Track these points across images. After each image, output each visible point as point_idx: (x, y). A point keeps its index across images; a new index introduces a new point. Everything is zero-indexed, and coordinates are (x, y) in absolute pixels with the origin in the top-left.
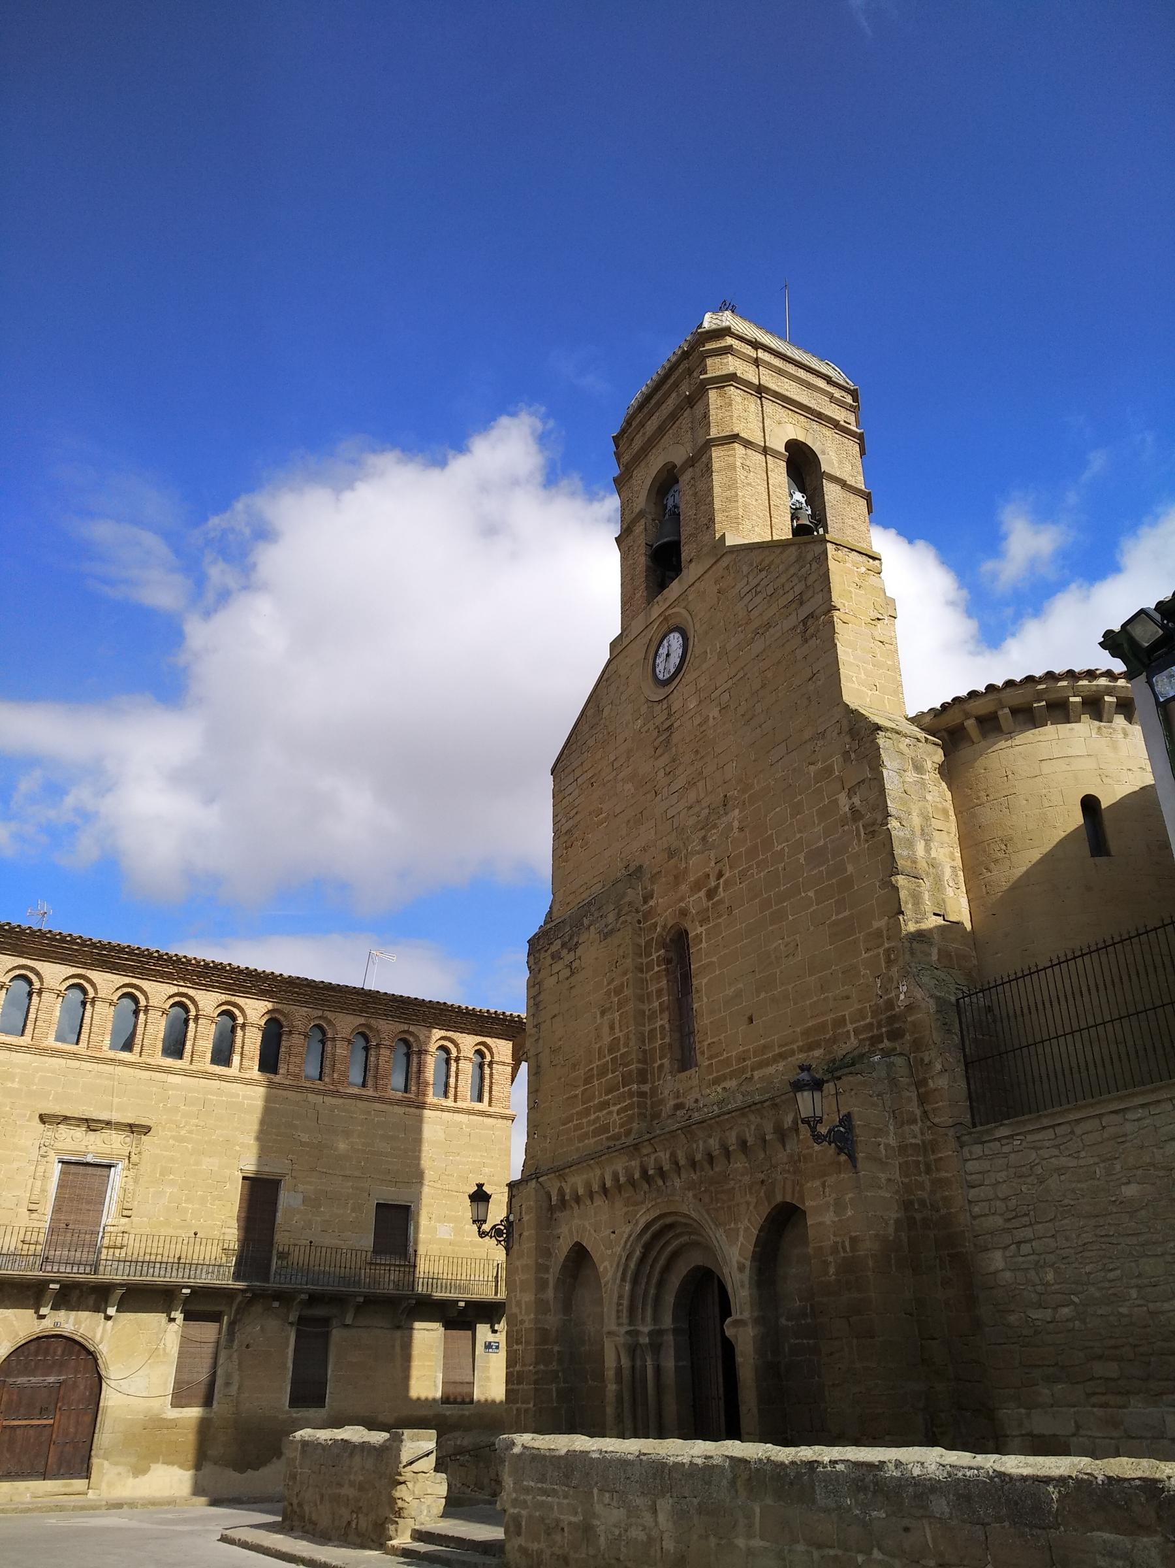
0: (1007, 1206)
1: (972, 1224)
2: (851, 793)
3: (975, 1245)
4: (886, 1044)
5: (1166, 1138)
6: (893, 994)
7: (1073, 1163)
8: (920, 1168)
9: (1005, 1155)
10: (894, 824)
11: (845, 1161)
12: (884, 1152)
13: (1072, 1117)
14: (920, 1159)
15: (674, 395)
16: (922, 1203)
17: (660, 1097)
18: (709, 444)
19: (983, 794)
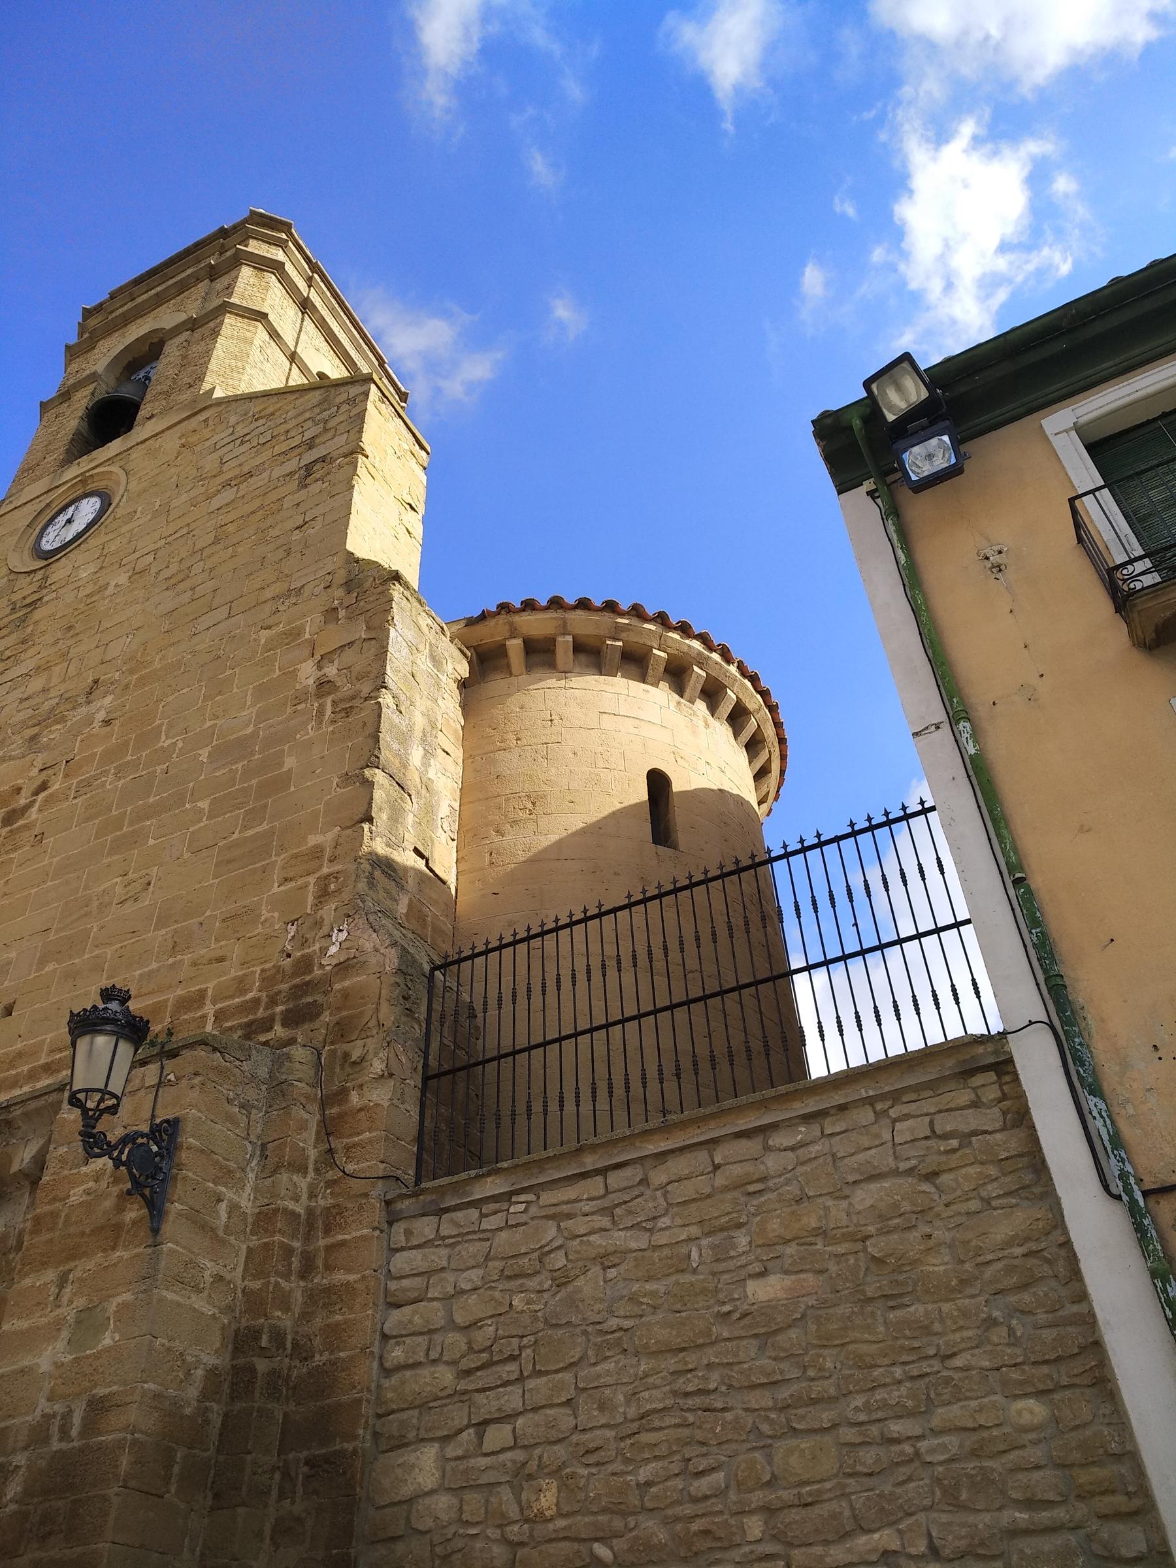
0: (469, 1343)
1: (379, 1387)
3: (376, 1435)
4: (279, 1031)
5: (858, 1177)
6: (317, 947)
7: (637, 1241)
8: (290, 1264)
9: (489, 1235)
10: (388, 701)
11: (134, 1223)
12: (224, 1215)
13: (651, 1148)
14: (296, 1244)
16: (278, 1337)
18: (226, 308)
19: (511, 737)
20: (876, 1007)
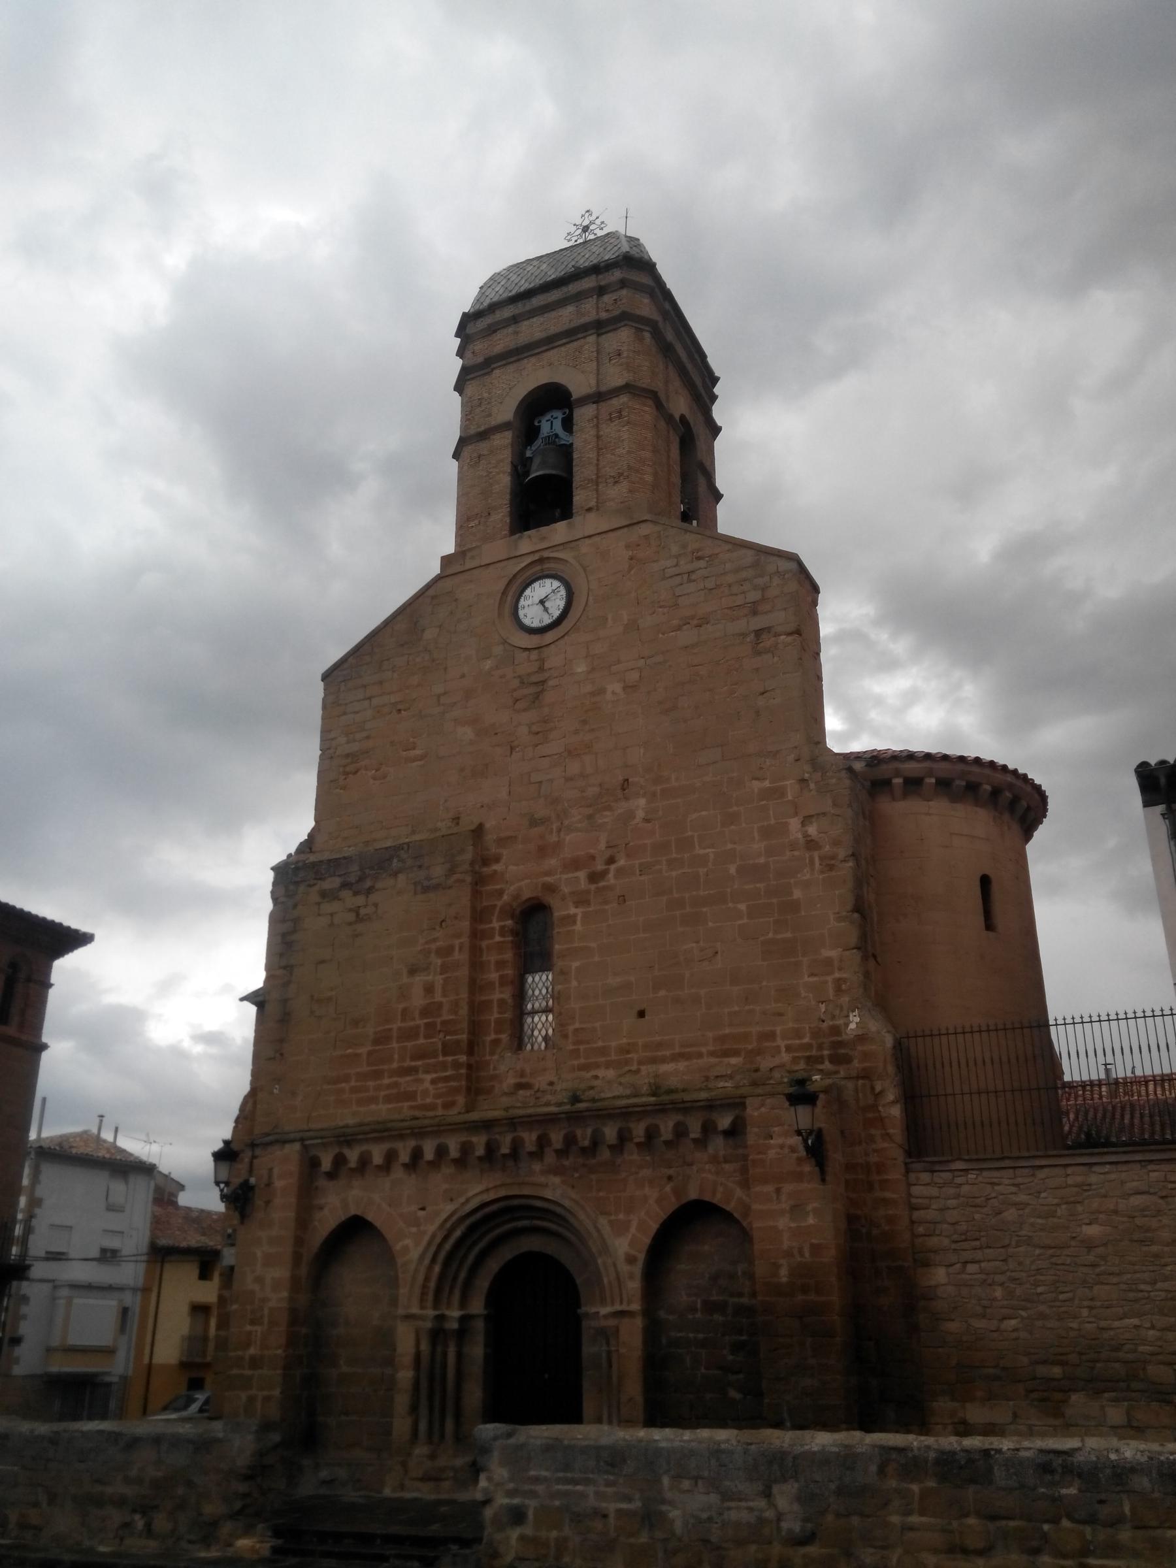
2: (807, 820)
13: (1038, 1162)
15: (570, 309)
17: (492, 1072)
20: (1096, 1057)
